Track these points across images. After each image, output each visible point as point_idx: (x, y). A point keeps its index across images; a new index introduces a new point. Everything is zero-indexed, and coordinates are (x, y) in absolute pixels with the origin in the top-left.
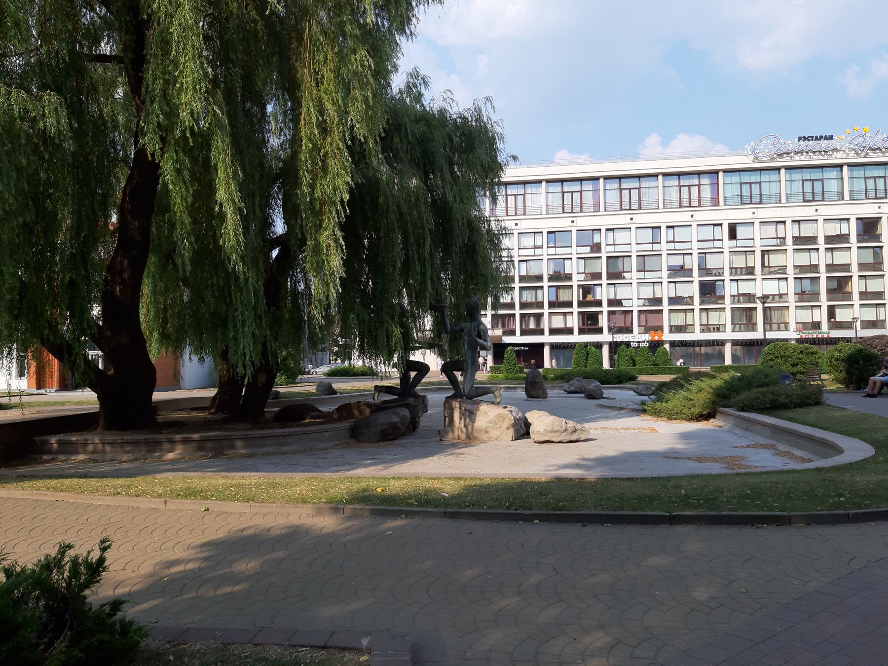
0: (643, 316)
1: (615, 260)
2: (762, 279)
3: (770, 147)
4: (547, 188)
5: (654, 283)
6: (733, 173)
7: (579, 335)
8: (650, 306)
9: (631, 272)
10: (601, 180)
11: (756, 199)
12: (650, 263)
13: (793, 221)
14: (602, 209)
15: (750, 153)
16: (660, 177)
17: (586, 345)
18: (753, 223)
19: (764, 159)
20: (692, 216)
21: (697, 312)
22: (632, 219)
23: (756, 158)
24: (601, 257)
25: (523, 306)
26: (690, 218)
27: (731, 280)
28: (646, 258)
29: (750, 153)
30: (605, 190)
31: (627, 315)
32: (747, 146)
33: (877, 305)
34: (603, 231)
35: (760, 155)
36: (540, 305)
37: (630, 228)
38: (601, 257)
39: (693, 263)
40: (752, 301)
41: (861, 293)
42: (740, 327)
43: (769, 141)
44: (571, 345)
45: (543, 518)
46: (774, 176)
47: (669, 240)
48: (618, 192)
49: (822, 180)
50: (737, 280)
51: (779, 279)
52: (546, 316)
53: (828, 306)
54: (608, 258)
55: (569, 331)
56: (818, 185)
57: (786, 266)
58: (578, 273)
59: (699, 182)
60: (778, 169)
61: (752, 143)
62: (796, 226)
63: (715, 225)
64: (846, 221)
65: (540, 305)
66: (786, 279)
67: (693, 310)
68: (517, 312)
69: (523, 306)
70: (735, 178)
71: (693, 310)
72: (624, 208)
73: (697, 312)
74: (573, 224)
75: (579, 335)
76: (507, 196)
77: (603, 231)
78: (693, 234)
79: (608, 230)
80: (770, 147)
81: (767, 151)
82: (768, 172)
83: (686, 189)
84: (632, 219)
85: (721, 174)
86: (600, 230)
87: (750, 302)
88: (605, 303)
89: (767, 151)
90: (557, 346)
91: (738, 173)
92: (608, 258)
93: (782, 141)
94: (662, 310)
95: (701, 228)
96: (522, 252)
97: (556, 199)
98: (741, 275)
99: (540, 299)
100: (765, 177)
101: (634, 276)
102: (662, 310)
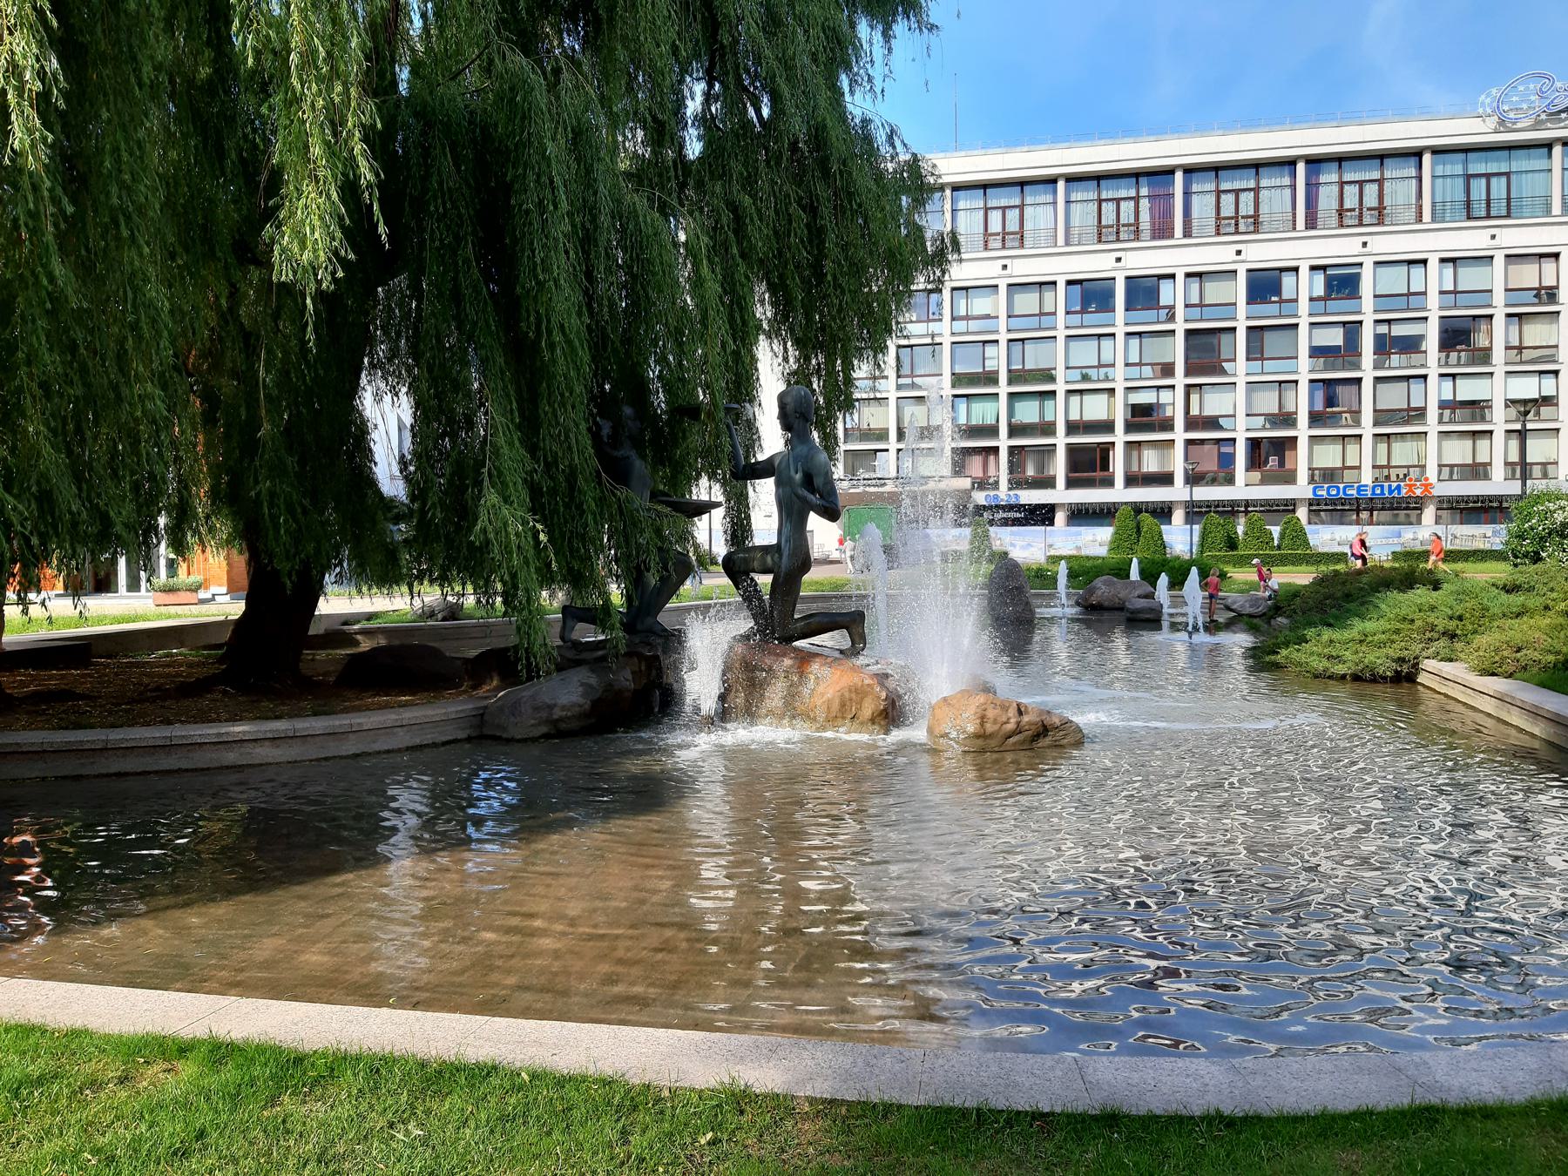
0: (1383, 447)
1: (1213, 339)
2: (1507, 372)
3: (1533, 98)
4: (1067, 193)
5: (1280, 382)
6: (1532, 151)
7: (1126, 487)
8: (1271, 429)
9: (1234, 360)
10: (948, 192)
11: (1499, 207)
12: (1271, 341)
13: (1443, 260)
14: (1427, 216)
15: (1489, 111)
16: (1061, 184)
17: (1138, 508)
18: (1492, 257)
19: (1519, 126)
20: (1365, 244)
21: (1367, 441)
22: (1239, 253)
23: (1502, 122)
24: (1174, 331)
25: (1014, 431)
26: (1358, 249)
27: (1442, 375)
28: (1029, 346)
29: (1489, 111)
30: (1068, 202)
31: (1479, 442)
32: (1483, 97)
33: (1474, 433)
34: (1180, 278)
35: (1512, 115)
36: (1047, 429)
37: (1235, 272)
38: (1174, 331)
39: (997, 359)
40: (1478, 418)
41: (1443, 405)
42: (1451, 473)
43: (1532, 86)
44: (1109, 509)
45: (149, 773)
46: (1535, 161)
47: (1315, 295)
48: (1460, 182)
49: (1508, 174)
50: (1454, 376)
51: (1541, 372)
52: (1303, 445)
53: (1248, 439)
54: (1189, 333)
55: (1166, 479)
56: (1499, 186)
57: (1557, 346)
58: (1127, 365)
59: (1138, 192)
60: (1548, 145)
61: (1494, 91)
62: (1449, 270)
63: (1411, 262)
64: (1553, 259)
65: (1047, 429)
66: (1425, 377)
67: (1360, 436)
68: (1003, 442)
69: (1014, 431)
70: (1455, 166)
71: (1360, 436)
72: (1476, 214)
73: (1367, 441)
74: (1119, 264)
75: (1126, 487)
76: (1100, 201)
77: (1180, 278)
78: (1496, 277)
79: (1188, 275)
80: (1533, 98)
81: (1525, 106)
82: (1526, 151)
83: (1230, 198)
84: (1239, 253)
85: (1427, 158)
86: (1054, 283)
87: (1473, 420)
88: (1061, 428)
89: (1525, 106)
90: (1080, 511)
91: (1461, 156)
92: (1189, 333)
93: (1558, 84)
94: (1296, 438)
95: (1382, 270)
96: (1015, 322)
97: (1083, 215)
98: (1458, 365)
99: (1049, 418)
100: (1520, 162)
101: (1240, 368)
102: (1296, 438)
